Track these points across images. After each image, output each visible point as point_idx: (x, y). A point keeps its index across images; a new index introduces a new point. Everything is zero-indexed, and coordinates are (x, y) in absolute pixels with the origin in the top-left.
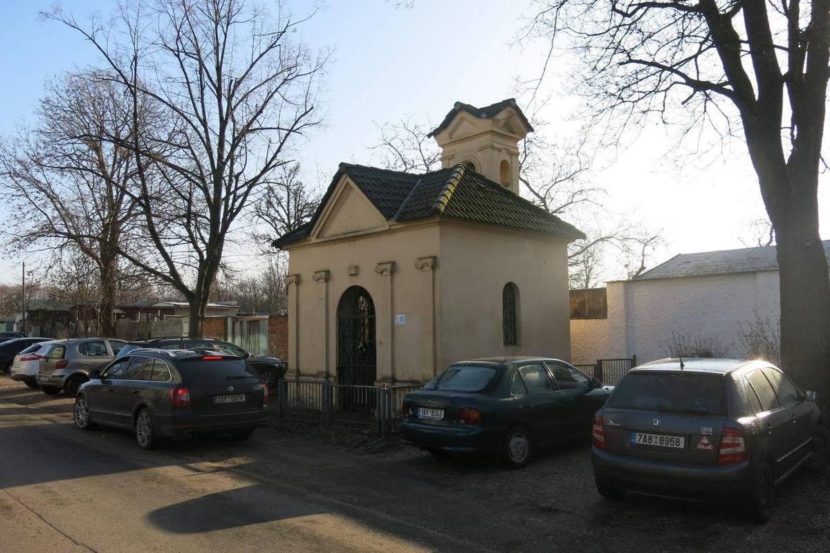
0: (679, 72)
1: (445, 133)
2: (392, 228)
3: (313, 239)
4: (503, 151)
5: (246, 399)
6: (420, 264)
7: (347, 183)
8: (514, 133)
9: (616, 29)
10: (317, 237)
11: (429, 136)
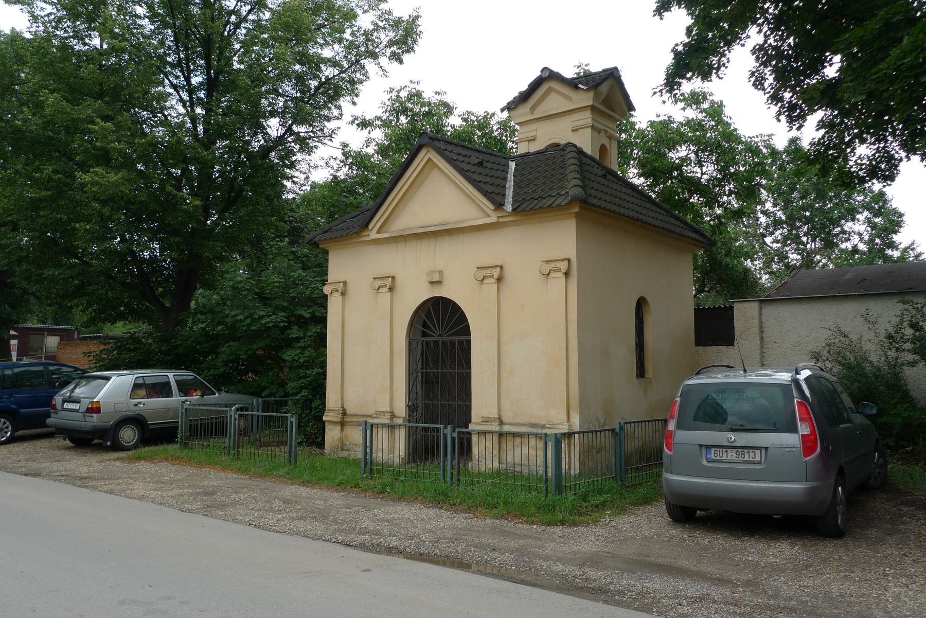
2: (501, 220)
3: (373, 235)
4: (603, 133)
6: (547, 268)
7: (429, 159)
8: (614, 111)
10: (379, 232)
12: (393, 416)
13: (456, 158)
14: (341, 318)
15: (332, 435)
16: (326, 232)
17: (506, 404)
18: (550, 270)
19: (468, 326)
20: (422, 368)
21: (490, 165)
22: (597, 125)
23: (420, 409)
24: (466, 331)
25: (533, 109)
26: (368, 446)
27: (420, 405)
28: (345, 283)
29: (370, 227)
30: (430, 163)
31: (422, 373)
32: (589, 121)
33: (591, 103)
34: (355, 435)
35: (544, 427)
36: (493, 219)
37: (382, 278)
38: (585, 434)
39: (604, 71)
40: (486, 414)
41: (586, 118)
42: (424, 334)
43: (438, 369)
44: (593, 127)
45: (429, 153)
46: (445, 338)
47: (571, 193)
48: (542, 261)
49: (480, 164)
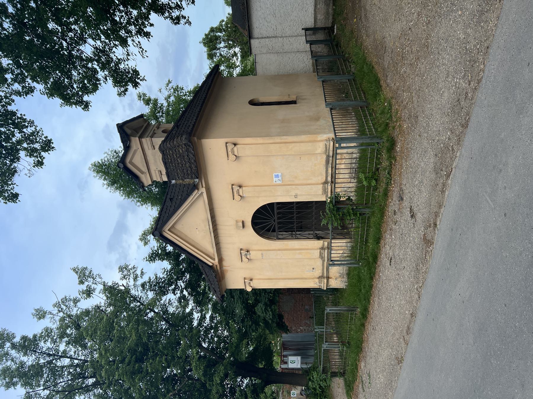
2: (204, 186)
6: (237, 197)
7: (169, 230)
10: (214, 259)
12: (322, 248)
13: (167, 214)
15: (335, 283)
16: (215, 291)
17: (314, 180)
18: (233, 154)
19: (269, 204)
20: (294, 231)
22: (150, 135)
24: (271, 205)
25: (142, 173)
29: (211, 264)
30: (173, 230)
31: (296, 231)
32: (148, 139)
33: (137, 138)
34: (335, 271)
35: (328, 156)
36: (203, 190)
39: (119, 132)
40: (320, 192)
41: (146, 141)
42: (274, 231)
43: (294, 222)
44: (152, 137)
45: (165, 231)
46: (276, 218)
48: (228, 160)
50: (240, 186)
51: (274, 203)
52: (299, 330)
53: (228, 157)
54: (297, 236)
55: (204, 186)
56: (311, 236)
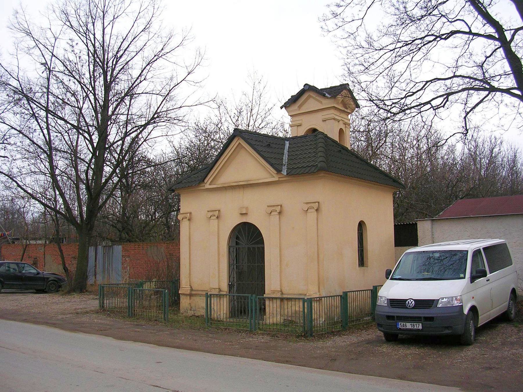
0: (456, 76)
1: (295, 107)
2: (281, 179)
3: (207, 186)
4: (341, 122)
5: (422, 327)
6: (306, 207)
9: (433, 38)
11: (281, 108)
14: (188, 233)
15: (184, 302)
18: (308, 208)
20: (237, 263)
21: (274, 146)
23: (235, 286)
24: (262, 241)
25: (300, 107)
26: (208, 306)
27: (235, 284)
28: (190, 213)
29: (205, 181)
31: (237, 266)
34: (201, 302)
36: (276, 179)
37: (212, 211)
38: (325, 298)
42: (237, 243)
47: (319, 165)
49: (269, 145)
50: (280, 213)
51: (395, 225)
52: (125, 266)
53: (306, 203)
54: (232, 266)
55: (281, 179)
56: (232, 279)
